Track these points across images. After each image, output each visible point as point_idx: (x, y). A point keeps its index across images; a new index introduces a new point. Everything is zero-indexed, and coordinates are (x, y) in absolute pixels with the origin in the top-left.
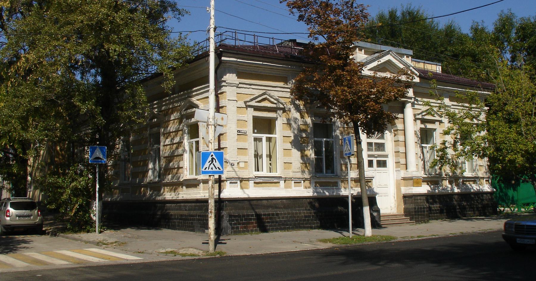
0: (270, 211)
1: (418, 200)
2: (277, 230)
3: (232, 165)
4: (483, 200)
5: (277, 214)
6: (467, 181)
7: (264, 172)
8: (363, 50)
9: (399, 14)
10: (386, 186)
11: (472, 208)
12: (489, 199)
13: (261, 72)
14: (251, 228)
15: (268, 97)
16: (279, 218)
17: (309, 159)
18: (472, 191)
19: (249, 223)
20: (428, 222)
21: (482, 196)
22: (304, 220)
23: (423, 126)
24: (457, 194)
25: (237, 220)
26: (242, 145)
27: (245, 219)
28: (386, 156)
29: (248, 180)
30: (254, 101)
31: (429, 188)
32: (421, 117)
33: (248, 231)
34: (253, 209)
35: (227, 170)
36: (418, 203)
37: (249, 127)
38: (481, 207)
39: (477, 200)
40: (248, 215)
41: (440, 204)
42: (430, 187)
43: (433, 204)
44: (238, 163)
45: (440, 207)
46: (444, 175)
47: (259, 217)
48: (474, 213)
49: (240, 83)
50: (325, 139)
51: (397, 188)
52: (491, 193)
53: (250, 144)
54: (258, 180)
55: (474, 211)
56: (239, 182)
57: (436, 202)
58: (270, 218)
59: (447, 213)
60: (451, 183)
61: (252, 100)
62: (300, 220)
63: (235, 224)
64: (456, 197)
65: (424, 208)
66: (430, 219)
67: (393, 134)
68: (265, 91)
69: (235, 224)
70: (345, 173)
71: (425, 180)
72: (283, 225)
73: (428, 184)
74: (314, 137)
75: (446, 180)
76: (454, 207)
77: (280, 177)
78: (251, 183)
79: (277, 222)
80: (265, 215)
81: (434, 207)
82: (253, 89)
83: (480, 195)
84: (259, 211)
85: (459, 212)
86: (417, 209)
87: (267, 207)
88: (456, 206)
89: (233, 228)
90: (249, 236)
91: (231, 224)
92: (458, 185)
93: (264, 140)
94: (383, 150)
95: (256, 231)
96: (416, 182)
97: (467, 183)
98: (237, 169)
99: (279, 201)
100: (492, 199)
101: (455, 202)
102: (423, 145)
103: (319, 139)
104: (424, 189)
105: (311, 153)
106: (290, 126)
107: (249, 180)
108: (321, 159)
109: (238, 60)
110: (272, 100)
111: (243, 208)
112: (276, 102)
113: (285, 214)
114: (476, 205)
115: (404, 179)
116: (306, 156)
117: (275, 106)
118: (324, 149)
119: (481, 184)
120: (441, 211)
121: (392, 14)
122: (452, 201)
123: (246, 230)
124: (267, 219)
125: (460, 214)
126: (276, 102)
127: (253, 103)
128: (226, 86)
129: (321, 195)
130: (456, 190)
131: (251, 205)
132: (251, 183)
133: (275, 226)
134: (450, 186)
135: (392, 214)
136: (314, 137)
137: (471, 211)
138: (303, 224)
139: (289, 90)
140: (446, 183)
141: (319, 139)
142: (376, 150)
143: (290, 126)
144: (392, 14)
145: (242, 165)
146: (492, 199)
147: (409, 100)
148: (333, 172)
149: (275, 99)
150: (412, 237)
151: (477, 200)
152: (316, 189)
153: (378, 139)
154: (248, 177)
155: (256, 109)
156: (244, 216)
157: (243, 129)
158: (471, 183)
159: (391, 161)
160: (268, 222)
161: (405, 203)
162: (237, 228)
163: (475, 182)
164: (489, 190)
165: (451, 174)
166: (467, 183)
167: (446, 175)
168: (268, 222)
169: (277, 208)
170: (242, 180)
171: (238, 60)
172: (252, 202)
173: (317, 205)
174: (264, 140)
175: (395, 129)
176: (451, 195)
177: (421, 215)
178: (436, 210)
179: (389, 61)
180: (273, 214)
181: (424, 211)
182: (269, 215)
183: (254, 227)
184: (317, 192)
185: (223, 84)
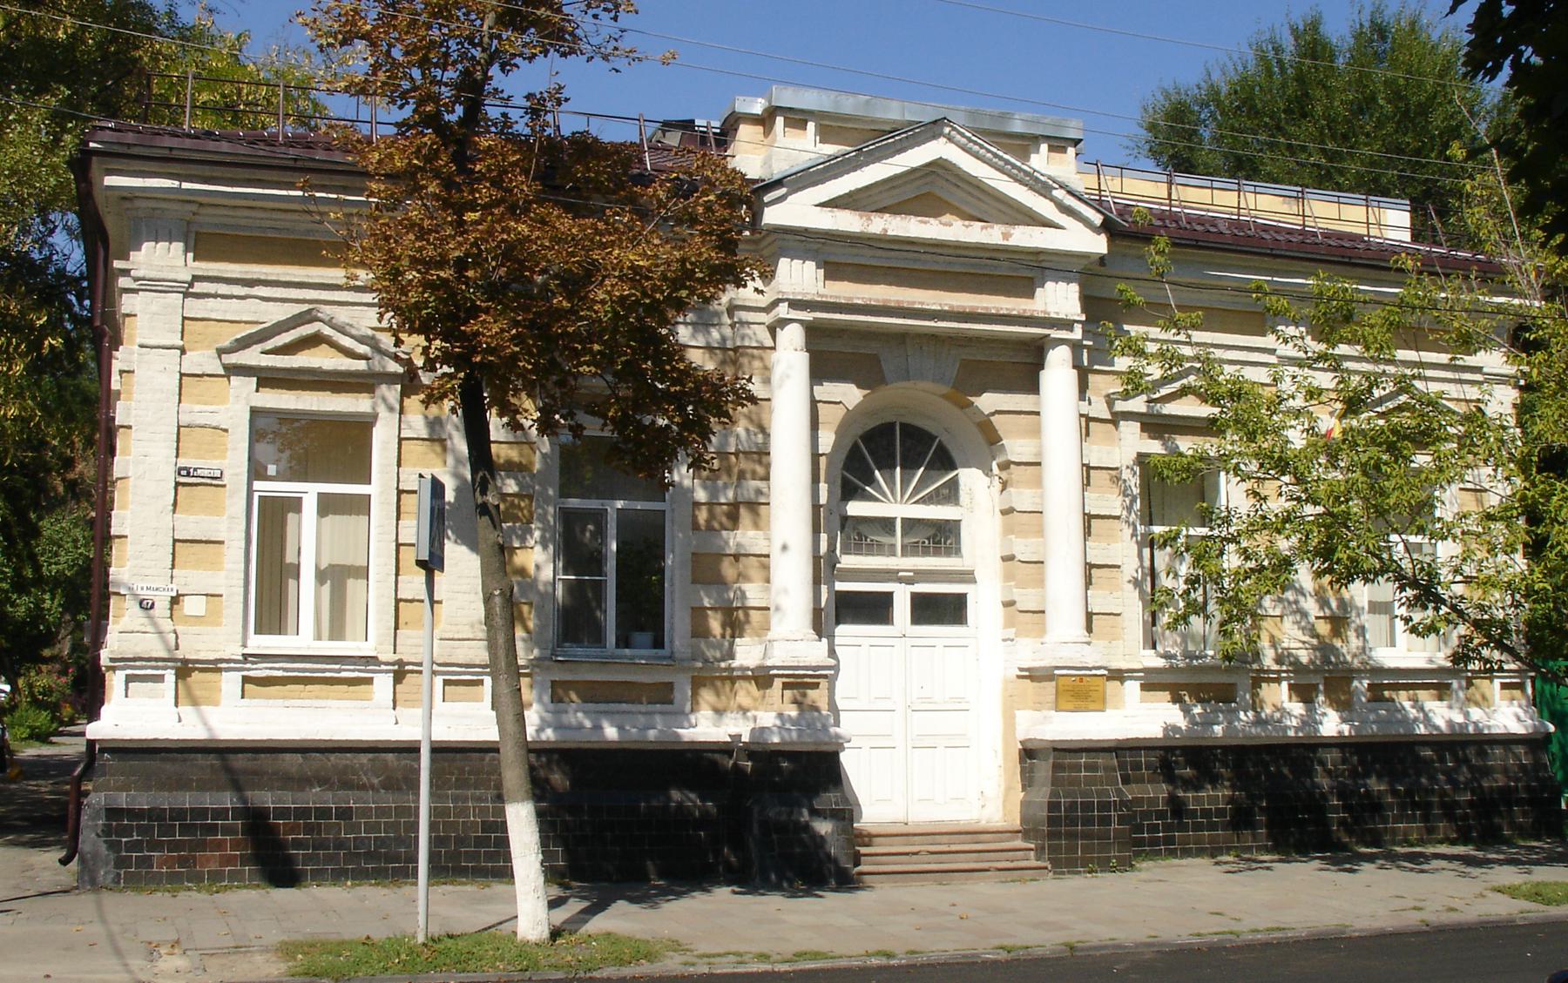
0: (314, 797)
1: (1077, 768)
2: (338, 876)
3: (146, 606)
4: (1486, 772)
5: (345, 814)
6: (1396, 687)
7: (303, 639)
8: (811, 126)
9: (1301, 27)
10: (959, 707)
11: (1417, 805)
12: (1522, 767)
13: (308, 232)
14: (214, 867)
15: (327, 331)
16: (355, 828)
17: (529, 583)
18: (1421, 730)
19: (202, 846)
20: (1126, 865)
21: (1482, 754)
22: (480, 842)
23: (1155, 447)
24: (1339, 743)
25: (142, 830)
26: (190, 525)
27: (185, 829)
28: (967, 577)
29: (215, 667)
30: (258, 348)
31: (1181, 721)
32: (1143, 409)
33: (197, 879)
34: (237, 787)
35: (120, 627)
36: (1074, 782)
37: (234, 459)
38: (1471, 803)
39: (1448, 773)
40: (202, 813)
41: (1233, 787)
42: (1186, 711)
43: (1198, 788)
44: (175, 601)
45: (1231, 800)
46: (1268, 661)
47: (257, 824)
48: (1430, 830)
49: (196, 278)
50: (620, 504)
51: (1005, 718)
52: (1536, 743)
53: (229, 520)
54: (261, 671)
55: (1426, 818)
56: (170, 676)
57: (1214, 780)
58: (309, 829)
59: (1270, 825)
60: (1304, 693)
61: (243, 344)
62: (460, 841)
63: (133, 846)
64: (1331, 756)
65: (1104, 806)
66: (1137, 854)
67: (997, 485)
68: (306, 307)
69: (133, 846)
70: (719, 646)
71: (1156, 679)
72: (370, 856)
73: (1176, 699)
74: (564, 493)
75: (1278, 681)
76: (1316, 805)
77: (371, 660)
78: (230, 682)
79: (340, 844)
80: (283, 813)
81: (1197, 800)
82: (259, 297)
83: (1471, 752)
84: (266, 799)
85: (1342, 822)
86: (1088, 808)
87: (303, 782)
88: (1323, 796)
89: (121, 863)
90: (193, 898)
91: (113, 846)
92: (1344, 706)
93: (310, 506)
94: (954, 550)
95: (234, 876)
96: (1079, 688)
97: (1403, 699)
98: (167, 625)
99: (364, 758)
100: (1538, 766)
101: (1324, 782)
102: (855, 508)
103: (593, 504)
104: (1146, 717)
105: (538, 559)
106: (445, 449)
107: (220, 670)
108: (599, 587)
109: (186, 185)
110: (346, 342)
111: (181, 784)
112: (363, 349)
113: (382, 812)
114: (1443, 793)
115: (1033, 675)
116: (522, 572)
117: (361, 365)
118: (614, 547)
119: (1484, 702)
120: (1240, 819)
121: (1313, 45)
122: (1310, 773)
123: (185, 874)
124: (293, 829)
125: (1350, 833)
126: (363, 349)
127: (252, 357)
128: (135, 291)
129: (574, 740)
130: (1331, 724)
131: (228, 770)
132: (230, 682)
133: (330, 859)
134: (1298, 708)
135: (983, 825)
136: (564, 493)
137: (1413, 819)
138: (474, 856)
139: (368, 298)
140: (1279, 697)
141: (593, 504)
142: (909, 550)
143: (445, 449)
144: (1313, 45)
145: (192, 606)
146: (1538, 766)
147: (1056, 334)
148: (658, 643)
149: (361, 340)
150: (764, 957)
151: (1448, 773)
152: (556, 713)
153: (922, 501)
154: (212, 657)
155: (268, 379)
156: (179, 814)
157: (205, 464)
158: (1422, 694)
159: (984, 601)
160: (298, 844)
161: (1028, 780)
162: (146, 862)
163: (1442, 691)
164: (1518, 729)
165: (1304, 657)
166: (1403, 699)
167: (1279, 660)
168: (298, 844)
169: (347, 785)
170: (184, 669)
171: (186, 185)
172: (240, 762)
173: (558, 779)
174: (310, 506)
175: (1001, 459)
176: (1305, 751)
177: (1085, 836)
178: (1206, 813)
179: (939, 168)
180: (324, 813)
181: (1106, 821)
182: (303, 813)
183: (229, 860)
184: (558, 727)
185: (123, 282)
